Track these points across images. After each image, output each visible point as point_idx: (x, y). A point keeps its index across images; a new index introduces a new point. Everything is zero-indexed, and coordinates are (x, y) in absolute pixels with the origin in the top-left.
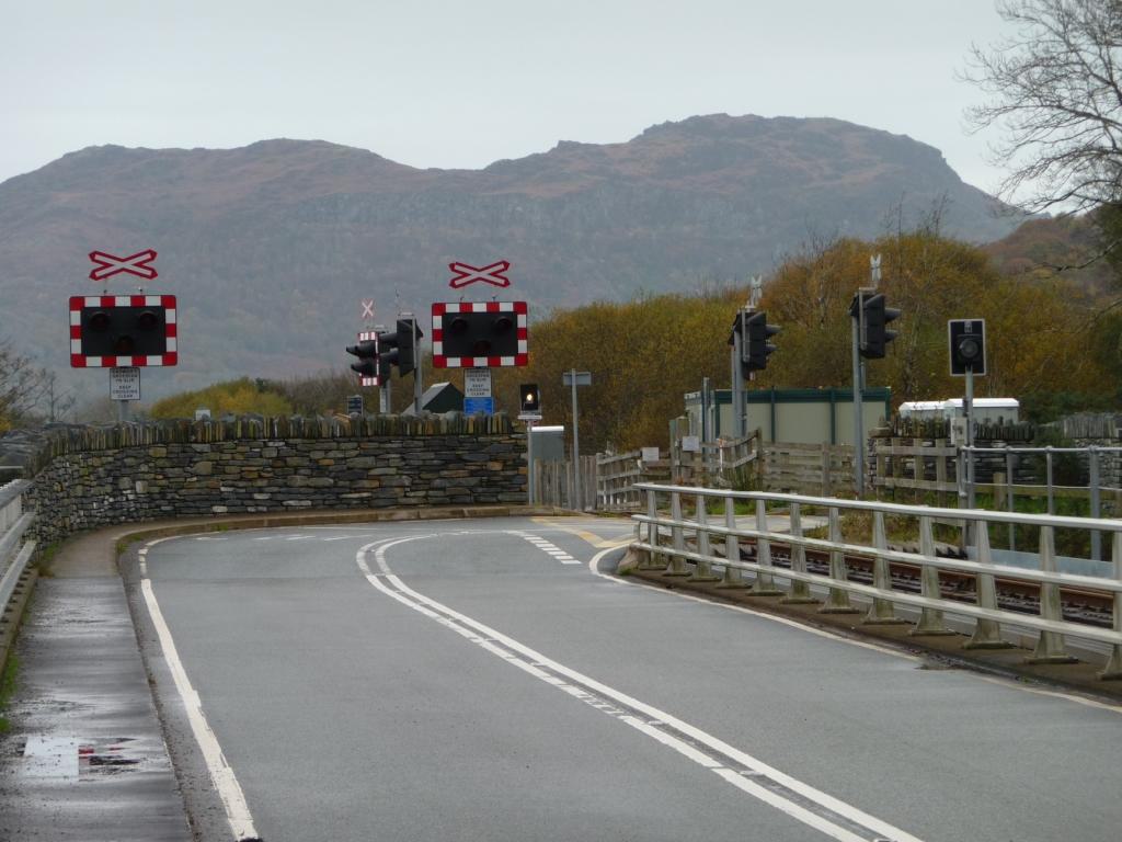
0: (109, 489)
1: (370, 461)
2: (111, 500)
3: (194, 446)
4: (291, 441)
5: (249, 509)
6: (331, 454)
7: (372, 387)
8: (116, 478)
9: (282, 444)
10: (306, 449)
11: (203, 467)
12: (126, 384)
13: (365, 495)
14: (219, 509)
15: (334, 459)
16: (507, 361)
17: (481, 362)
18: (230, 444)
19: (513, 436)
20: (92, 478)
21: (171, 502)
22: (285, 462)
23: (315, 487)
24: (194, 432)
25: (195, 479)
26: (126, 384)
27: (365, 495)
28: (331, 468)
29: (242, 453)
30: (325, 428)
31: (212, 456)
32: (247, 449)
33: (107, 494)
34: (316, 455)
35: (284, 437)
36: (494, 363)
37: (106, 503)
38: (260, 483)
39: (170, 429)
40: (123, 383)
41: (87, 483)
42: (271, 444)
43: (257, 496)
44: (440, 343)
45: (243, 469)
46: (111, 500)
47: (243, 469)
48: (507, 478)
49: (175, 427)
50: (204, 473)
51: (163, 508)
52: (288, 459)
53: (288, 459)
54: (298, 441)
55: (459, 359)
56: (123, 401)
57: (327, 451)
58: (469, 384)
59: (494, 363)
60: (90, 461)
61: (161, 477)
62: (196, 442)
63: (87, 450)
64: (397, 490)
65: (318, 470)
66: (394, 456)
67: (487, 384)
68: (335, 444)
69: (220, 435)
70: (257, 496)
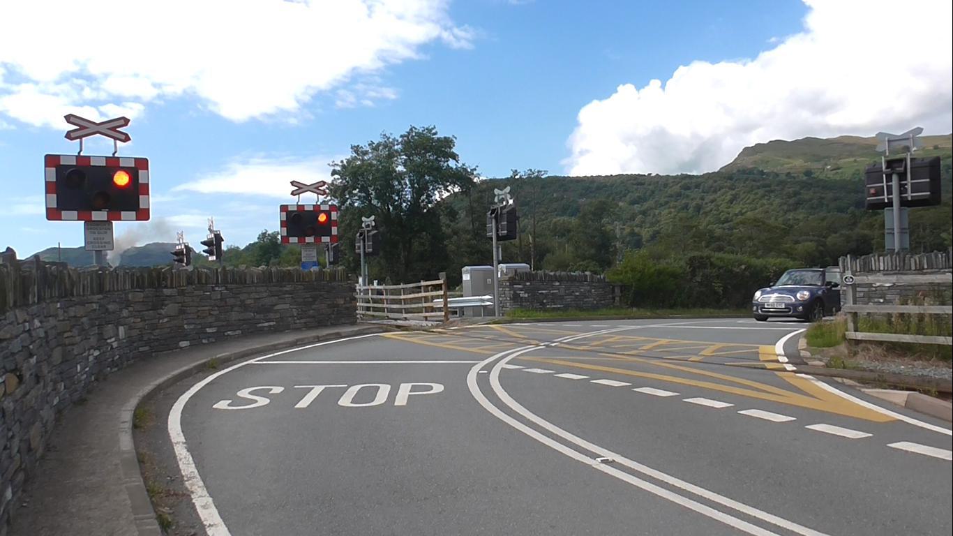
0: (93, 340)
1: (274, 299)
2: (97, 353)
3: (164, 290)
4: (229, 286)
5: (204, 341)
6: (252, 296)
7: (213, 261)
8: (100, 326)
9: (223, 288)
10: (237, 292)
11: (170, 308)
12: (99, 236)
13: (272, 323)
14: (184, 344)
15: (254, 299)
16: (326, 239)
17: (310, 240)
18: (190, 288)
19: (349, 282)
20: (75, 332)
21: (147, 343)
22: (226, 302)
23: (243, 320)
24: (165, 279)
25: (166, 320)
26: (99, 236)
27: (272, 323)
28: (252, 306)
29: (198, 296)
30: (248, 278)
31: (179, 299)
32: (201, 293)
33: (92, 347)
34: (243, 297)
35: (225, 282)
36: (318, 240)
37: (91, 358)
38: (210, 319)
39: (146, 275)
40: (96, 236)
41: (67, 341)
42: (217, 289)
43: (209, 330)
44: (285, 229)
45: (199, 309)
46: (97, 353)
47: (199, 309)
48: (347, 309)
49: (150, 275)
50: (172, 314)
51: (141, 349)
52: (228, 300)
53: (228, 300)
54: (233, 286)
55: (336, 234)
56: (96, 251)
57: (249, 293)
58: (304, 253)
59: (318, 240)
60: (72, 311)
61: (139, 320)
62: (166, 287)
63: (66, 294)
64: (290, 319)
65: (245, 307)
66: (287, 296)
67: (314, 253)
68: (254, 288)
69: (184, 282)
70: (209, 330)
